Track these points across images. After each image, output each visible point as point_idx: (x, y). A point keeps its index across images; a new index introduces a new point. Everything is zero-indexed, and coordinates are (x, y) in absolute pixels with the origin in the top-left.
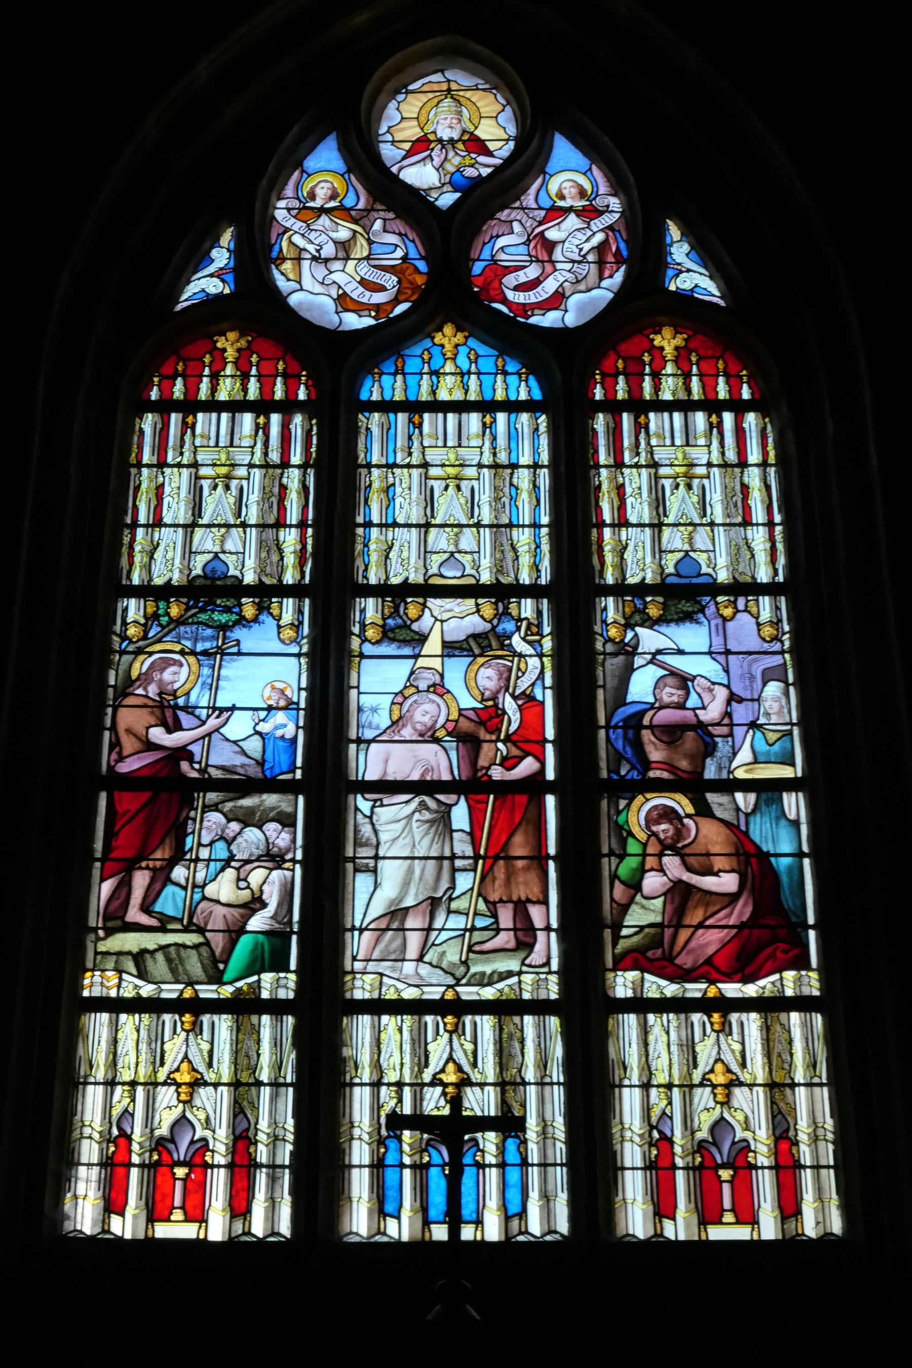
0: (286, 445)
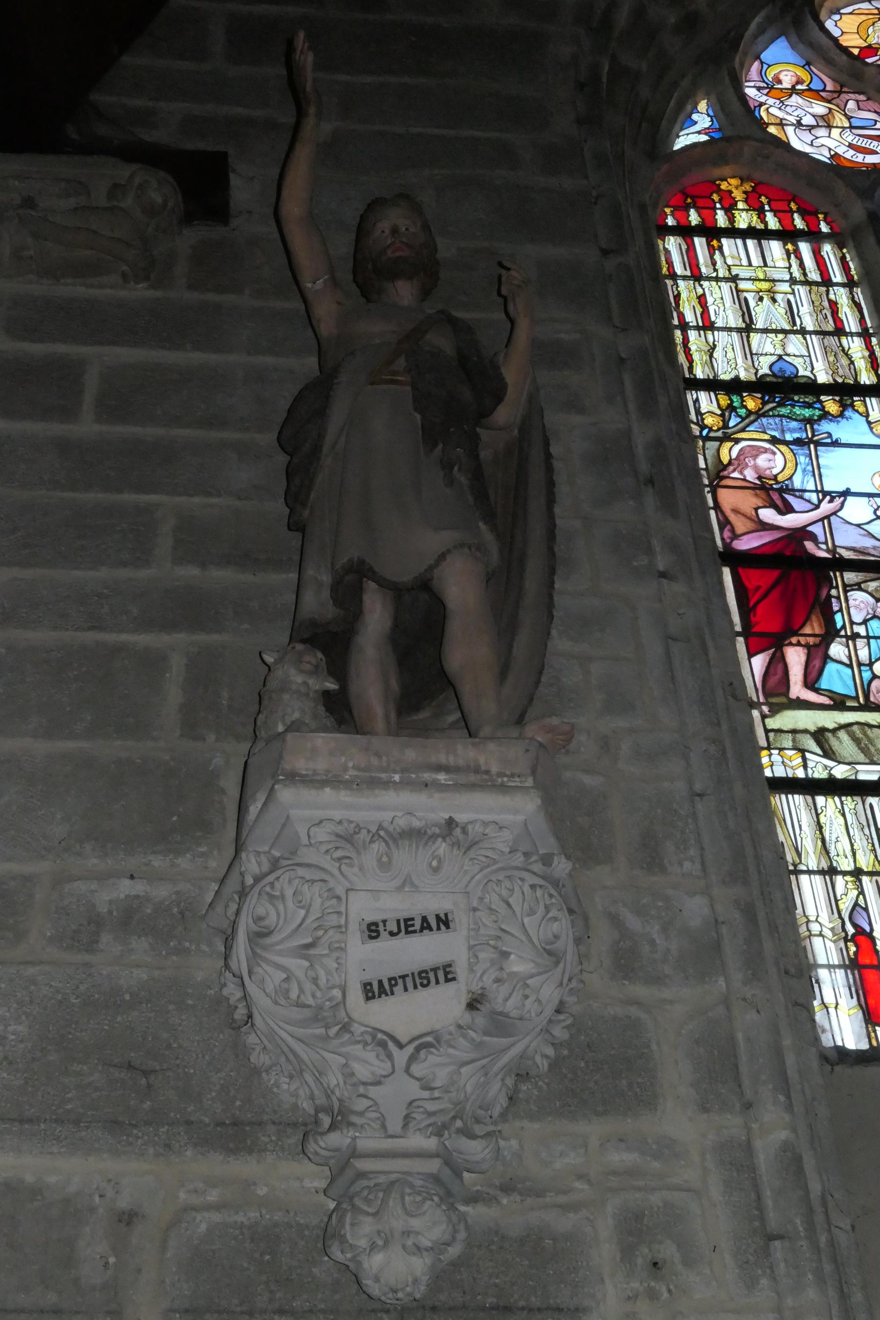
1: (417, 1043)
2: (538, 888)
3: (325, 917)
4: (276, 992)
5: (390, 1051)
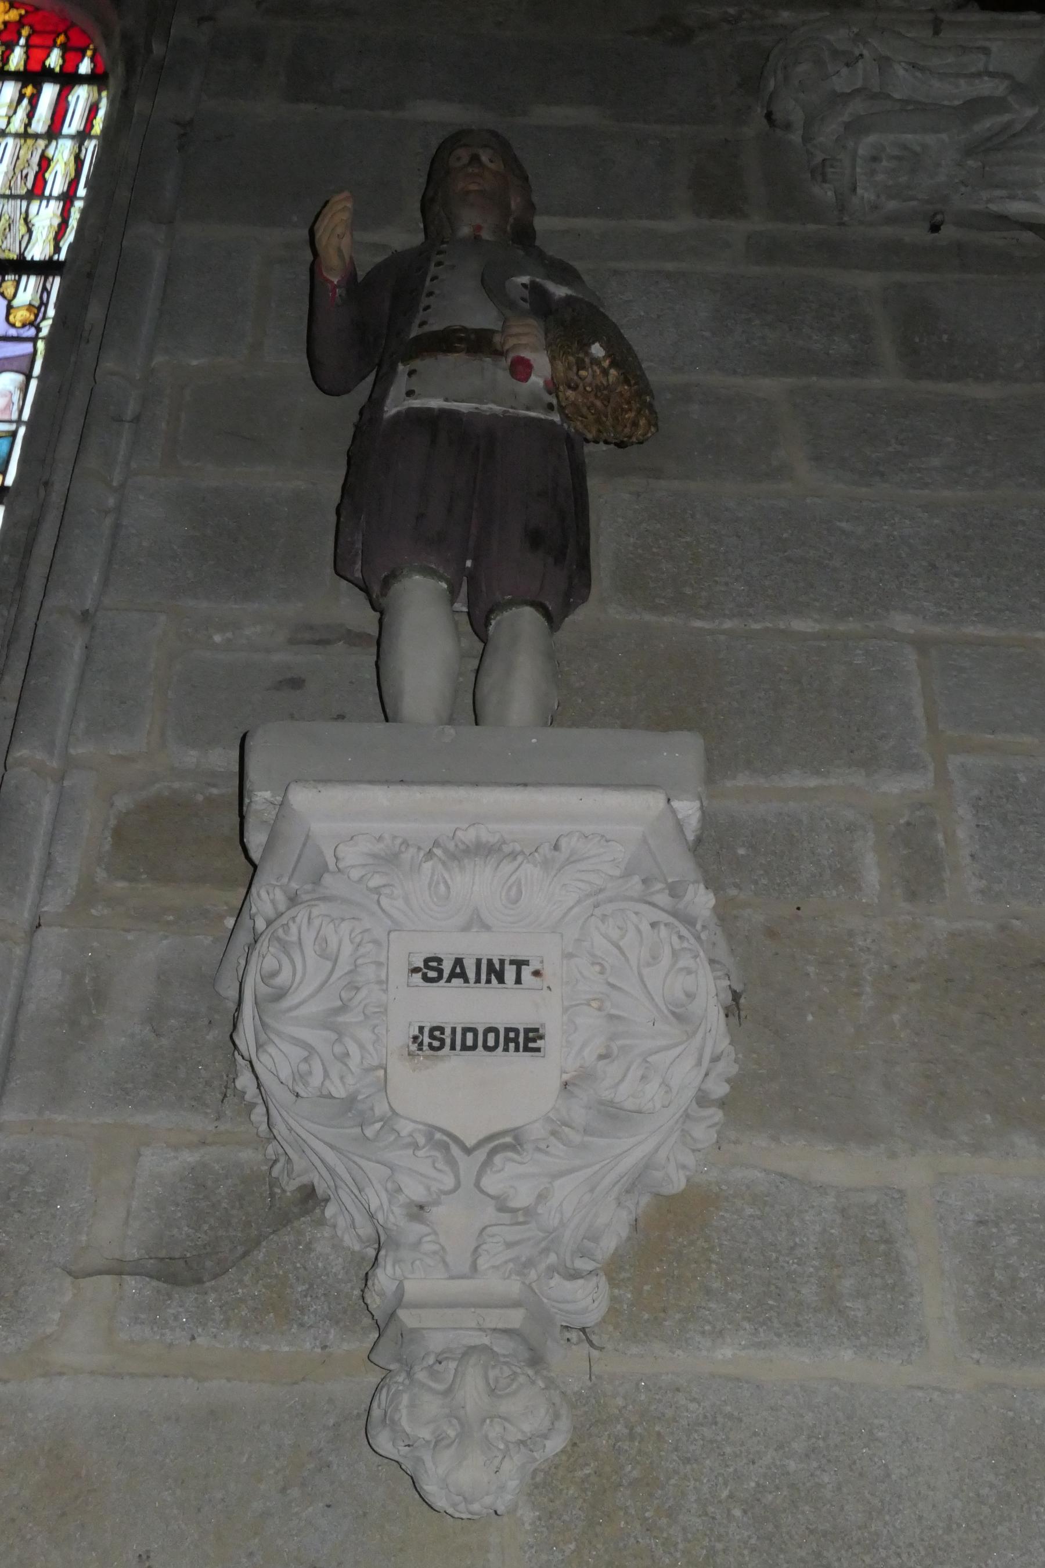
0: (92, 116)
1: (492, 1145)
2: (662, 927)
3: (359, 969)
4: (294, 1079)
5: (453, 1157)
